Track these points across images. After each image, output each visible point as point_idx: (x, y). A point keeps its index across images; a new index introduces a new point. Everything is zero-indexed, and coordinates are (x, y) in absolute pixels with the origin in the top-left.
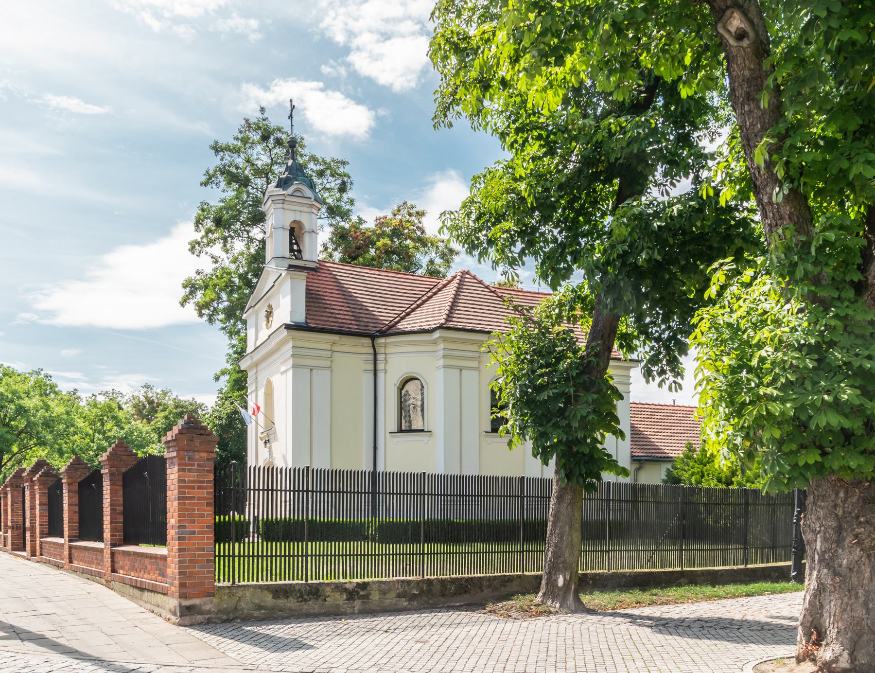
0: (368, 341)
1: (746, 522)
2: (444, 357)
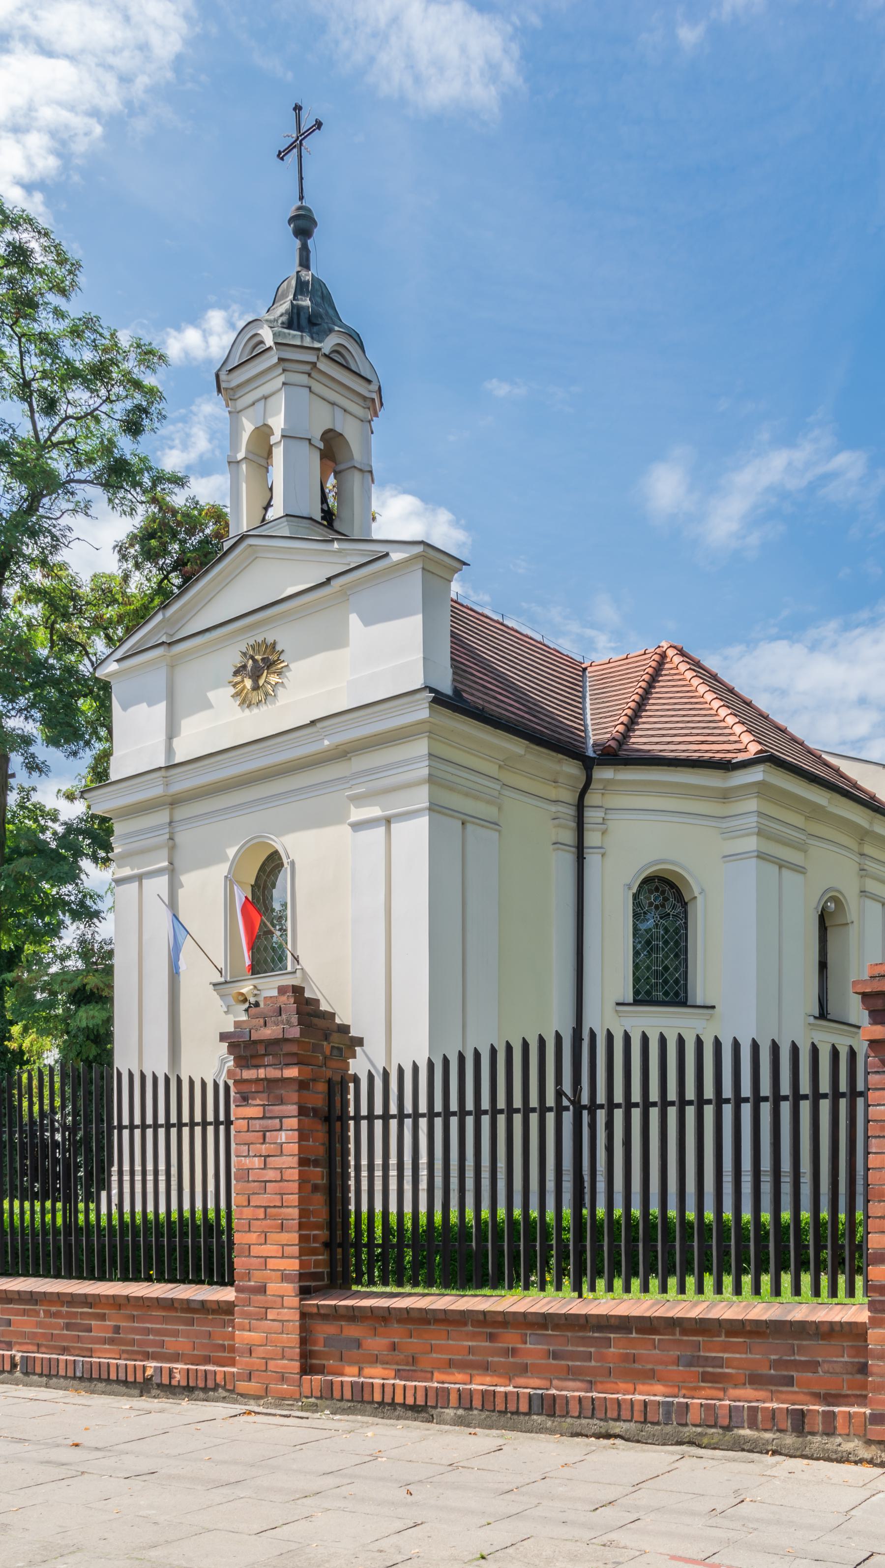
0: (571, 769)
1: (76, 1011)
2: (760, 833)
